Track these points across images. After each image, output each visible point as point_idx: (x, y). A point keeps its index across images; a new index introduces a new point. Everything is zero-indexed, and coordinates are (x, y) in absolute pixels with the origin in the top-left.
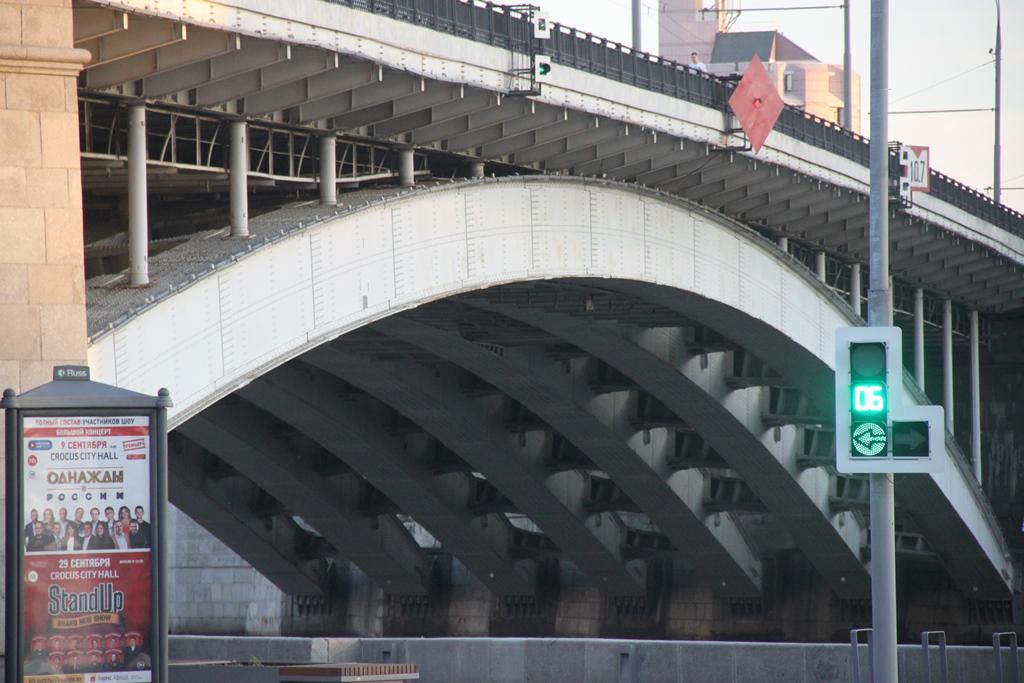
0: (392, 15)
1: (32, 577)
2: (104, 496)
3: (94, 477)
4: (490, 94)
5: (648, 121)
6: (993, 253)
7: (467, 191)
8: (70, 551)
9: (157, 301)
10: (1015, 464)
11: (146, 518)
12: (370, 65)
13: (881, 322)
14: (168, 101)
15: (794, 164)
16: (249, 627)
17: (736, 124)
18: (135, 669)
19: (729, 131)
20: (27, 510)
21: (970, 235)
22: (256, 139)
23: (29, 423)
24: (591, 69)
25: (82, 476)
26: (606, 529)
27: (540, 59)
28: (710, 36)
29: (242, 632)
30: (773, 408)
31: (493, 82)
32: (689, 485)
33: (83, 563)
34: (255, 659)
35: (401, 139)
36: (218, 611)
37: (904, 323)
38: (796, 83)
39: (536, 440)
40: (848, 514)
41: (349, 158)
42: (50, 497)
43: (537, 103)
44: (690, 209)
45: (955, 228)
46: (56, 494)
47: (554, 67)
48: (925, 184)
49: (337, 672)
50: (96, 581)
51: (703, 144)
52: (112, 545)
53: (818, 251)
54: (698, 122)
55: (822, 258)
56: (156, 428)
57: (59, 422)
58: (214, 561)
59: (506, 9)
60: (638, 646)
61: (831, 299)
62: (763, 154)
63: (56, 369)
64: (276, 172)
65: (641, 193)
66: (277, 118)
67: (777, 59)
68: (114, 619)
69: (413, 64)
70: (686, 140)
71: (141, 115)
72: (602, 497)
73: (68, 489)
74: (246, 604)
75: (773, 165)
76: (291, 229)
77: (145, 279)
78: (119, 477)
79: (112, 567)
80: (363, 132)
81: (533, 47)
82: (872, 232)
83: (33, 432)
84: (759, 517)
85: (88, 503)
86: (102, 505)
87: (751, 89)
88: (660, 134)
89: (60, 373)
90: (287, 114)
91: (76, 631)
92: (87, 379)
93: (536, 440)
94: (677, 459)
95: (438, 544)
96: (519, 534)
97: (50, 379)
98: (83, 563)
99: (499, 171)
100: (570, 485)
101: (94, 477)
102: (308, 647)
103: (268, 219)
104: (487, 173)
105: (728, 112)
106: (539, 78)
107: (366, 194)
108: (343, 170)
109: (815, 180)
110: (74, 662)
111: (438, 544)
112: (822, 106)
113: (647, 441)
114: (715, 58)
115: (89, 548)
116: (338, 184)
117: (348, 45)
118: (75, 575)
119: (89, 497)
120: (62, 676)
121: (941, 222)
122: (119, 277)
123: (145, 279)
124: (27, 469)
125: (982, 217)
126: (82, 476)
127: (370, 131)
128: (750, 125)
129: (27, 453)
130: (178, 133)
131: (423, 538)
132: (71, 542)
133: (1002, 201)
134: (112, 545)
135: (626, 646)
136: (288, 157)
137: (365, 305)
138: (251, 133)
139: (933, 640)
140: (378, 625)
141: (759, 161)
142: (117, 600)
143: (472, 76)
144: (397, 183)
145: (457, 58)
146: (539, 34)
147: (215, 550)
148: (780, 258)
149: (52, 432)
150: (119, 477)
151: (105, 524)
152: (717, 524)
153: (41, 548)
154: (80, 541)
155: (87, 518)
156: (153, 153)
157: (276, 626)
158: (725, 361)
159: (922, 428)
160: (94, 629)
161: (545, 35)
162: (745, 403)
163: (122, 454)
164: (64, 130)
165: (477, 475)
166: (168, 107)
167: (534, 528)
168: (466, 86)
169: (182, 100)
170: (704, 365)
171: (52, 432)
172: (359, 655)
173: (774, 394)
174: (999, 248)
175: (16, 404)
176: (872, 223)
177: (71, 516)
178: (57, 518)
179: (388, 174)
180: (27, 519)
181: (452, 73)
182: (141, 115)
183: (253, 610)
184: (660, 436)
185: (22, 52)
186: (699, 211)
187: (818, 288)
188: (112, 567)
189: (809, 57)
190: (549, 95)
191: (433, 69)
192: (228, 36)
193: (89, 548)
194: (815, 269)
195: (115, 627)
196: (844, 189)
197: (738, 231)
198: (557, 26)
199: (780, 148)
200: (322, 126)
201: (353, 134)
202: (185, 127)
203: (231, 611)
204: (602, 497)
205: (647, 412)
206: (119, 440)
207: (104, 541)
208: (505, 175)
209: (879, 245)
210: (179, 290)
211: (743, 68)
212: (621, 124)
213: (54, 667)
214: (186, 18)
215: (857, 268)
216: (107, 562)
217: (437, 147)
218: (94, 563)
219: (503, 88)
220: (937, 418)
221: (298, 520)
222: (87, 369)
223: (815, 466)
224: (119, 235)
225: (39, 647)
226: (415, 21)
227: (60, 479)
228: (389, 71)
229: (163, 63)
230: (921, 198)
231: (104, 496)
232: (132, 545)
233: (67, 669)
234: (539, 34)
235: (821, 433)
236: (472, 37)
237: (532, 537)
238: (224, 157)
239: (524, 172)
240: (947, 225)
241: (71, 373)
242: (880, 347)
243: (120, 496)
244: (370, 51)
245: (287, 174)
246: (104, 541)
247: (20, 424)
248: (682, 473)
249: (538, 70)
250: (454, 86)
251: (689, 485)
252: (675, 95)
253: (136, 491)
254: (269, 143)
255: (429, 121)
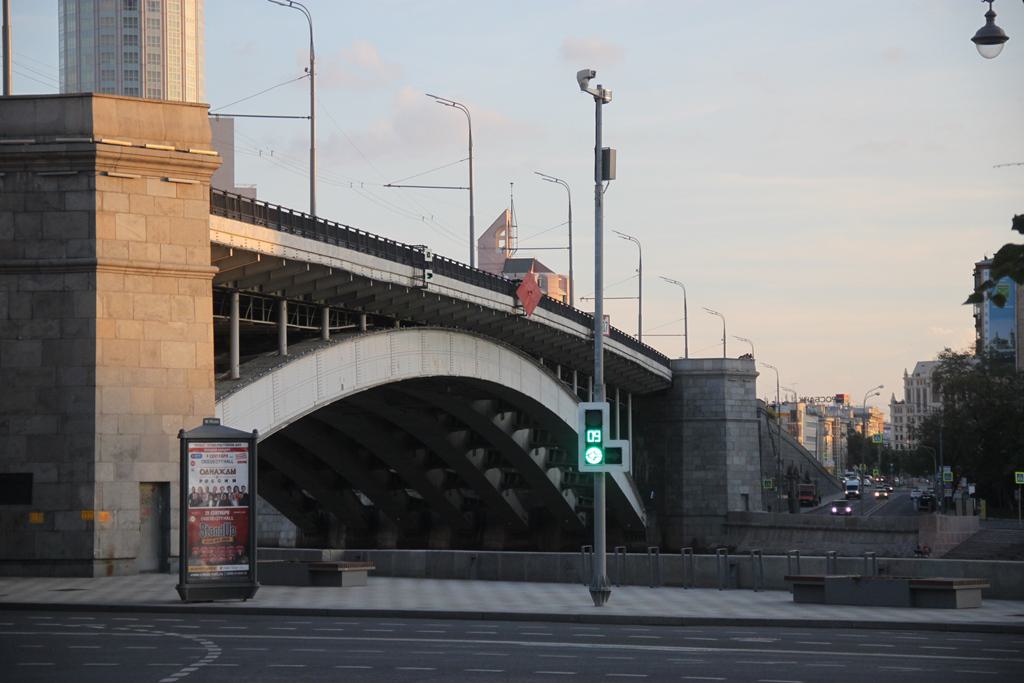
0: (357, 250)
1: (192, 519)
2: (226, 481)
3: (222, 472)
4: (403, 287)
5: (478, 301)
6: (639, 366)
7: (392, 334)
8: (211, 507)
9: (243, 387)
10: (647, 467)
11: (246, 491)
12: (347, 273)
13: (600, 400)
14: (250, 290)
15: (547, 322)
16: (280, 543)
17: (520, 303)
18: (241, 564)
19: (516, 306)
20: (190, 487)
21: (628, 357)
22: (291, 309)
23: (191, 445)
24: (452, 276)
25: (216, 471)
26: (454, 498)
27: (427, 271)
28: (503, 261)
29: (277, 546)
30: (535, 439)
31: (405, 282)
32: (494, 476)
33: (216, 513)
34: (297, 560)
35: (360, 309)
36: (266, 535)
37: (611, 399)
38: (544, 283)
39: (421, 454)
40: (570, 490)
41: (335, 318)
42: (201, 481)
43: (426, 292)
44: (497, 343)
45: (621, 354)
46: (204, 479)
47: (434, 275)
48: (608, 333)
49: (336, 566)
50: (222, 522)
51: (504, 313)
52: (230, 504)
53: (557, 364)
54: (501, 302)
55: (559, 368)
56: (250, 449)
57: (206, 445)
58: (264, 511)
59: (411, 247)
60: (479, 554)
61: (563, 387)
62: (533, 318)
63: (204, 420)
64: (300, 324)
65: (474, 335)
66: (301, 298)
67: (535, 271)
68: (231, 540)
69: (367, 273)
70: (496, 310)
71: (237, 297)
72: (452, 482)
73: (210, 477)
74: (280, 532)
75: (537, 323)
76: (307, 352)
77: (238, 376)
78: (234, 472)
79: (230, 515)
80: (342, 305)
81: (424, 265)
82: (596, 357)
83: (193, 450)
84: (527, 491)
85: (219, 484)
86: (226, 485)
87: (528, 287)
88: (483, 307)
89: (207, 422)
90: (305, 297)
91: (214, 545)
92: (219, 424)
93: (421, 454)
94: (488, 464)
95: (372, 504)
96: (412, 499)
97: (201, 424)
98: (216, 513)
99: (407, 324)
100: (437, 475)
101: (222, 472)
102: (321, 553)
103: (296, 347)
104: (401, 326)
105: (516, 298)
106: (427, 280)
107: (343, 335)
108: (332, 324)
109: (556, 330)
110: (212, 560)
111: (372, 504)
112: (556, 294)
113: (474, 455)
114: (505, 270)
115: (220, 505)
116: (330, 331)
117: (336, 264)
118: (212, 519)
119: (219, 481)
120: (207, 567)
121: (615, 351)
122: (224, 375)
123: (238, 376)
124: (190, 467)
125: (633, 349)
126: (216, 471)
127: (345, 305)
128: (526, 303)
129: (190, 459)
130: (254, 305)
131: (365, 500)
132: (211, 503)
133: (643, 341)
134: (230, 504)
135: (475, 554)
136: (261, 311)
137: (342, 388)
138: (288, 305)
139: (620, 551)
140: (342, 542)
141: (530, 321)
142: (233, 531)
143: (395, 279)
144: (357, 331)
145: (388, 270)
146: (427, 259)
147: (264, 506)
148: (540, 367)
149: (202, 450)
150: (234, 472)
151: (227, 494)
152: (507, 495)
153: (196, 505)
154: (215, 502)
155: (218, 491)
156: (241, 316)
157: (293, 543)
158: (512, 415)
159: (619, 450)
160: (222, 544)
161: (430, 260)
162: (522, 436)
163: (235, 461)
164: (206, 303)
165: (392, 471)
166: (250, 293)
167: (419, 496)
168: (392, 284)
169: (256, 290)
170: (503, 418)
171: (202, 450)
172: (345, 558)
173: (535, 433)
174: (641, 363)
175: (186, 436)
176: (596, 353)
177: (211, 490)
178: (204, 491)
179: (354, 326)
180: (190, 492)
181: (386, 277)
182: (237, 297)
183: (282, 535)
184: (481, 452)
185: (187, 268)
186: (479, 336)
187: (557, 382)
188: (230, 515)
189: (550, 271)
190: (432, 288)
191: (376, 275)
192: (280, 259)
193: (220, 505)
194: (556, 372)
195: (232, 544)
196: (570, 335)
197: (519, 354)
198: (435, 255)
199: (540, 315)
200: (322, 302)
201: (337, 306)
202: (257, 303)
203: (272, 535)
204: (452, 482)
205: (474, 442)
206: (235, 454)
207: (226, 502)
208: (410, 326)
209: (599, 364)
210: (254, 381)
211: (521, 276)
212: (465, 302)
213: (202, 562)
214: (260, 251)
215: (591, 378)
216: (228, 512)
217: (377, 312)
218: (222, 513)
219: (409, 285)
220: (626, 446)
221: (305, 492)
222: (219, 420)
223: (553, 467)
224: (225, 354)
225: (196, 553)
226: (368, 253)
227: (206, 473)
228: (355, 276)
229: (248, 272)
230: (605, 340)
231: (226, 481)
232: (240, 504)
233: (208, 563)
234: (427, 259)
235: (557, 451)
236: (395, 261)
237: (418, 501)
238: (276, 317)
239: (419, 325)
240: (618, 352)
241: (211, 421)
242: (599, 412)
243: (234, 481)
244: (347, 266)
245: (261, 319)
246: (226, 502)
247: (187, 446)
248: (491, 470)
249: (427, 276)
250: (386, 284)
251: (494, 476)
252: (491, 289)
253: (242, 479)
254: (297, 310)
255: (374, 300)
